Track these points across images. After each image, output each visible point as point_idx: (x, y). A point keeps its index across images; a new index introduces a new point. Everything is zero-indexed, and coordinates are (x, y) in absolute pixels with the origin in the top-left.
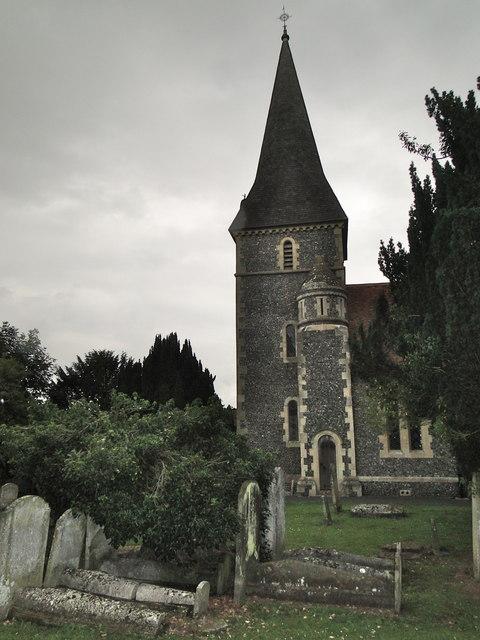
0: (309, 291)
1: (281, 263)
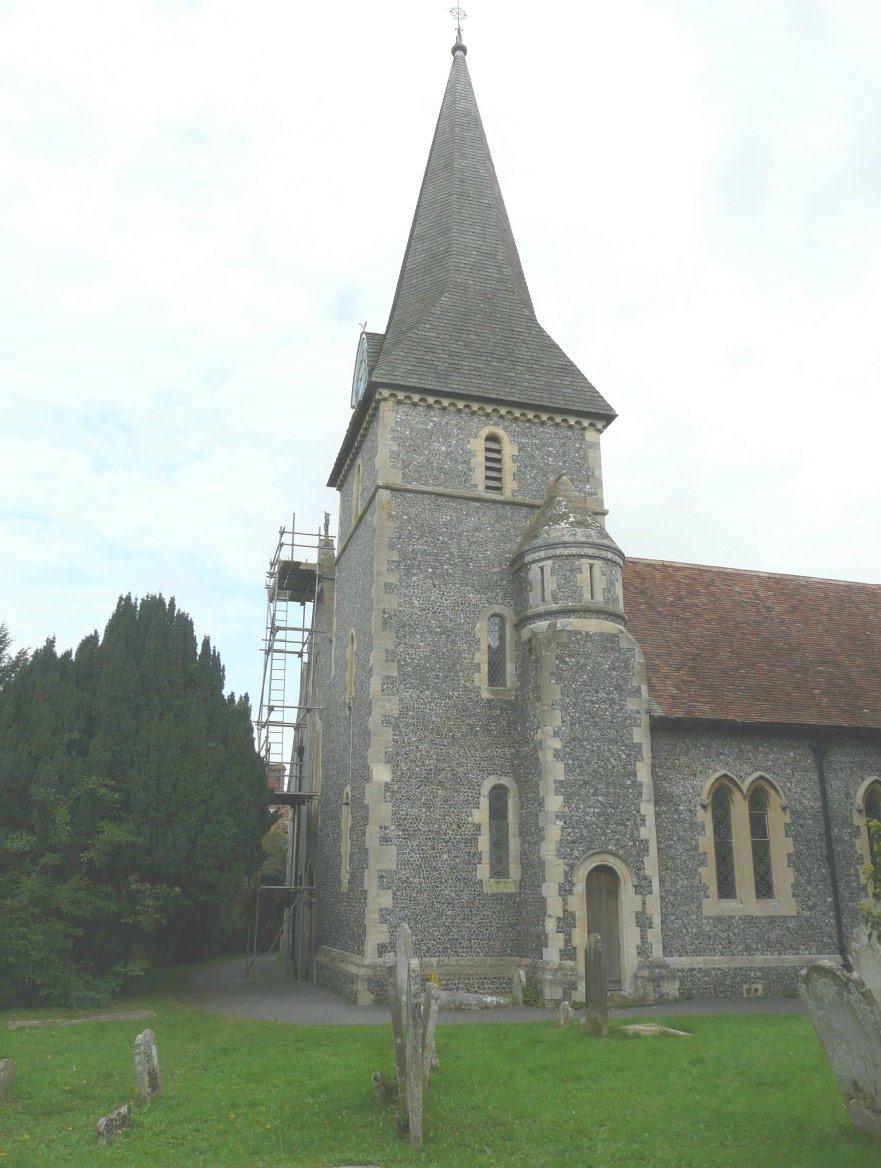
0: (565, 545)
1: (479, 476)
